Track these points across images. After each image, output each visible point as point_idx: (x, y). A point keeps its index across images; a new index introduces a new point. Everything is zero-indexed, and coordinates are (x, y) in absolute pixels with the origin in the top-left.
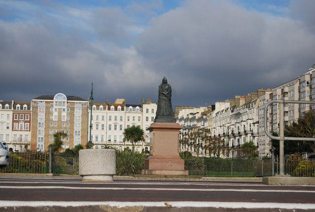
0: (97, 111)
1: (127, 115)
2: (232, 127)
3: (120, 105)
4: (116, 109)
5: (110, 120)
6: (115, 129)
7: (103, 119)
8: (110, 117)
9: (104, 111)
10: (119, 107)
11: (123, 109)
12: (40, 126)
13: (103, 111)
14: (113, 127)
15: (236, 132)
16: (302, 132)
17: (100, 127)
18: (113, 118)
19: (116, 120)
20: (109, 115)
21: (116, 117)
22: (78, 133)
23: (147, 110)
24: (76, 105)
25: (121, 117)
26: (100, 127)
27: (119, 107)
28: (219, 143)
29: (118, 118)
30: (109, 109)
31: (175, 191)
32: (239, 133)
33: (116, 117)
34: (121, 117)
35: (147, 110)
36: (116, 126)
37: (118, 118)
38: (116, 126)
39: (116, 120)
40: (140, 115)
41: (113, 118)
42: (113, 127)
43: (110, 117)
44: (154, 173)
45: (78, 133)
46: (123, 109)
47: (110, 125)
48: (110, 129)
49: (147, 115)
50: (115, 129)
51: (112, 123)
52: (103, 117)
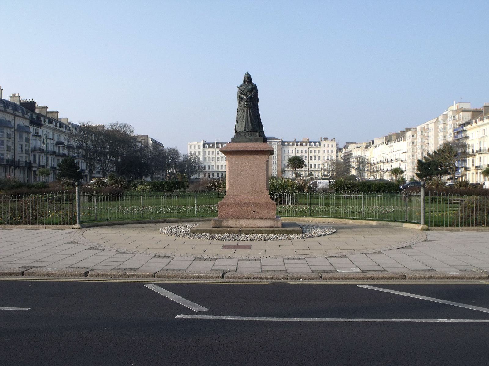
0: (301, 147)
1: (310, 149)
2: (386, 156)
3: (292, 142)
7: (306, 153)
8: (298, 151)
9: (293, 147)
10: (304, 144)
11: (306, 145)
12: (273, 159)
13: (305, 147)
14: (313, 158)
15: (389, 160)
17: (317, 158)
18: (313, 152)
19: (302, 153)
20: (297, 149)
21: (302, 151)
22: (274, 163)
23: (324, 145)
24: (273, 143)
25: (306, 151)
26: (317, 158)
27: (304, 144)
29: (304, 152)
30: (297, 145)
31: (7, 306)
32: (374, 163)
33: (302, 151)
34: (306, 151)
35: (324, 145)
36: (315, 157)
37: (304, 152)
38: (315, 157)
39: (302, 153)
40: (319, 149)
41: (313, 152)
42: (313, 158)
43: (298, 151)
44: (225, 223)
45: (274, 163)
46: (306, 145)
47: (311, 157)
48: (311, 159)
50: (315, 159)
51: (312, 155)
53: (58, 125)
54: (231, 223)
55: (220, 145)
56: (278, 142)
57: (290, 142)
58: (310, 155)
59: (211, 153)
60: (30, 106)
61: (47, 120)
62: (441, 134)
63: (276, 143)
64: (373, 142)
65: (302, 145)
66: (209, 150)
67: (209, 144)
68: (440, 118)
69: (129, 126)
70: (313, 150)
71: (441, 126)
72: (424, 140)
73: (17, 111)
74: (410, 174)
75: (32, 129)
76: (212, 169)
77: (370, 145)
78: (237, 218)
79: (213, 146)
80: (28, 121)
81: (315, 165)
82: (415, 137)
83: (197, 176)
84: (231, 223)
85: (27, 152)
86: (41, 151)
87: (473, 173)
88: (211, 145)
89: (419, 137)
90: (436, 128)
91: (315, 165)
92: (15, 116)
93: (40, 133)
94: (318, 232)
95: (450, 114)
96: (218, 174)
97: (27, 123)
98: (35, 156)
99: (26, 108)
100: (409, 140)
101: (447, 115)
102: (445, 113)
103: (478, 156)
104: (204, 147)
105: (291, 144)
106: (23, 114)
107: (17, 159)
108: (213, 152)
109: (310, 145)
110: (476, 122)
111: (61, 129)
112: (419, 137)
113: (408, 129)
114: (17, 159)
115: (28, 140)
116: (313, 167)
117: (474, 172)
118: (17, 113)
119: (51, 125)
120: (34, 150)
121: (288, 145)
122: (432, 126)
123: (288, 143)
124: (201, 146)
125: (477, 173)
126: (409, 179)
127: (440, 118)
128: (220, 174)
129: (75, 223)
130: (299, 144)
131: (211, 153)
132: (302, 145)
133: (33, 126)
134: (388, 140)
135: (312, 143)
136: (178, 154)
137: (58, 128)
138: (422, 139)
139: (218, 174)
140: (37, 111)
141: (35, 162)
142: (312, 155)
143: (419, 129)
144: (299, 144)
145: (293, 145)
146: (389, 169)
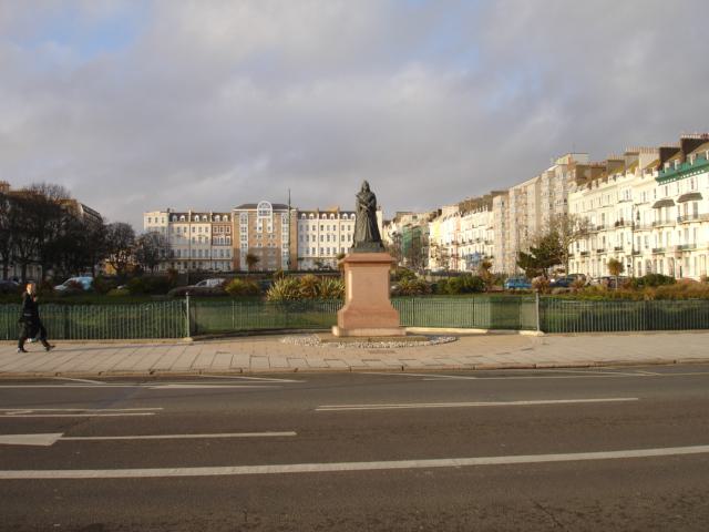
1: (193, 225)
15: (460, 242)
27: (332, 215)
36: (328, 237)
38: (328, 237)
44: (351, 333)
46: (336, 217)
54: (357, 332)
55: (197, 217)
57: (203, 214)
58: (342, 233)
62: (545, 202)
64: (440, 212)
65: (328, 217)
66: (156, 225)
67: (179, 215)
68: (545, 176)
70: (197, 226)
71: (545, 189)
72: (520, 210)
74: (504, 264)
76: (200, 256)
77: (435, 216)
78: (362, 327)
79: (186, 218)
81: (328, 250)
82: (506, 205)
84: (357, 332)
87: (578, 263)
88: (183, 217)
89: (512, 205)
90: (538, 191)
91: (328, 250)
94: (442, 340)
95: (559, 171)
96: (194, 263)
100: (497, 209)
101: (554, 172)
102: (551, 169)
103: (601, 235)
104: (171, 219)
105: (312, 215)
109: (341, 218)
110: (597, 185)
112: (512, 205)
113: (495, 194)
116: (325, 252)
117: (595, 258)
121: (308, 218)
122: (531, 188)
123: (308, 213)
124: (166, 219)
125: (600, 260)
126: (608, 271)
127: (545, 176)
128: (197, 263)
129: (182, 335)
130: (332, 215)
132: (328, 217)
134: (464, 209)
135: (345, 215)
136: (132, 232)
138: (517, 207)
139: (194, 263)
142: (324, 233)
143: (512, 194)
144: (324, 215)
145: (315, 217)
146: (466, 253)
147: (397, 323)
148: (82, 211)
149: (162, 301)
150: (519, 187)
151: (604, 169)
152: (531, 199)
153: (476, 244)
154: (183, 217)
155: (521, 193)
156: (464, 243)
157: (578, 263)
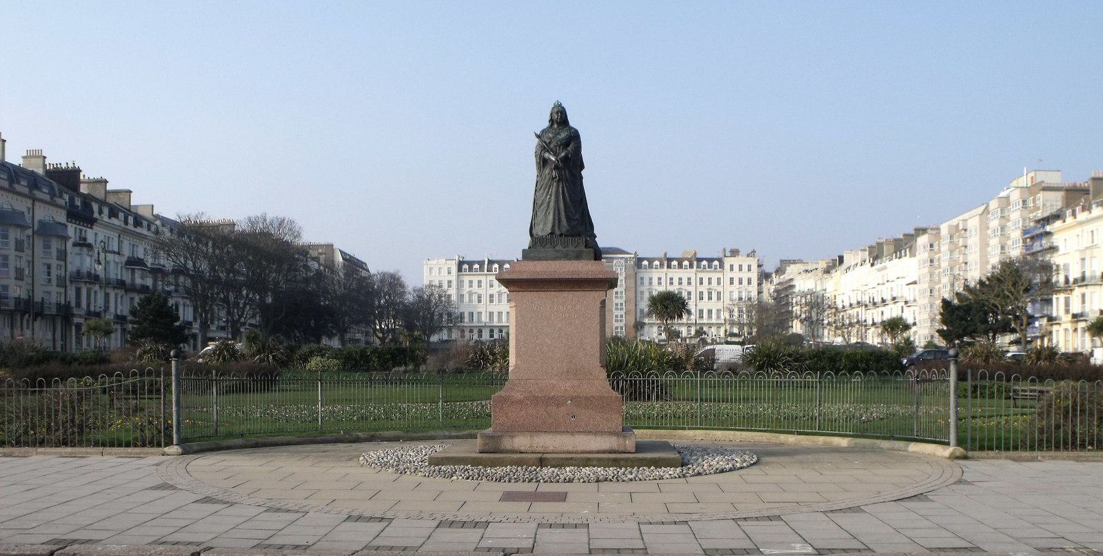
1: (700, 275)
4: (680, 266)
5: (701, 283)
6: (710, 298)
8: (671, 279)
12: (616, 297)
13: (659, 270)
14: (706, 296)
15: (878, 300)
16: (998, 296)
17: (714, 296)
18: (705, 281)
19: (680, 283)
21: (680, 279)
22: (619, 307)
23: (732, 267)
24: (615, 262)
26: (714, 296)
27: (686, 263)
28: (127, 431)
29: (685, 281)
30: (669, 267)
33: (680, 279)
35: (732, 267)
36: (710, 293)
37: (685, 281)
38: (710, 293)
40: (720, 275)
41: (705, 281)
42: (706, 296)
43: (671, 279)
44: (507, 443)
45: (619, 307)
46: (691, 266)
47: (701, 293)
48: (701, 298)
49: (750, 275)
50: (710, 298)
51: (704, 288)
52: (660, 279)
53: (131, 220)
54: (521, 442)
56: (626, 259)
57: (654, 259)
58: (700, 289)
59: (475, 284)
60: (68, 178)
61: (106, 210)
62: (995, 242)
63: (623, 261)
64: (841, 259)
65: (680, 266)
66: (471, 278)
67: (471, 264)
68: (994, 205)
69: (292, 222)
71: (994, 223)
72: (956, 255)
73: (39, 189)
75: (72, 230)
76: (479, 320)
77: (834, 266)
78: (534, 430)
80: (64, 213)
81: (710, 312)
82: (936, 248)
83: (444, 335)
84: (521, 442)
85: (62, 282)
86: (94, 278)
87: (1066, 330)
88: (476, 266)
89: (945, 248)
90: (984, 227)
91: (710, 312)
92: (34, 200)
93: (90, 240)
94: (718, 462)
95: (1015, 196)
96: (492, 331)
97: (61, 217)
98: (78, 291)
99: (60, 182)
100: (922, 255)
101: (1008, 198)
102: (1003, 194)
103: (1078, 291)
104: (460, 269)
105: (657, 263)
106: (53, 195)
107: (38, 298)
108: (480, 282)
109: (698, 267)
110: (1074, 214)
111: (139, 230)
112: (945, 248)
114: (38, 298)
115: (62, 255)
116: (705, 315)
117: (1069, 326)
118: (38, 194)
119: (114, 221)
120: (78, 277)
121: (650, 266)
123: (651, 261)
124: (454, 269)
127: (994, 205)
128: (496, 331)
129: (169, 443)
131: (475, 284)
133: (79, 225)
134: (875, 254)
135: (704, 263)
136: (402, 286)
137: (131, 227)
138: (951, 252)
139: (492, 331)
140: (84, 189)
141: (78, 305)
142: (704, 288)
143: (944, 229)
144: (675, 263)
145: (662, 265)
146: (878, 320)
147: (617, 422)
148: (341, 259)
149: (779, 385)
150: (954, 222)
151: (1085, 191)
152: (974, 240)
153: (891, 306)
154: (476, 266)
155: (959, 231)
156: (883, 301)
157: (1066, 330)
